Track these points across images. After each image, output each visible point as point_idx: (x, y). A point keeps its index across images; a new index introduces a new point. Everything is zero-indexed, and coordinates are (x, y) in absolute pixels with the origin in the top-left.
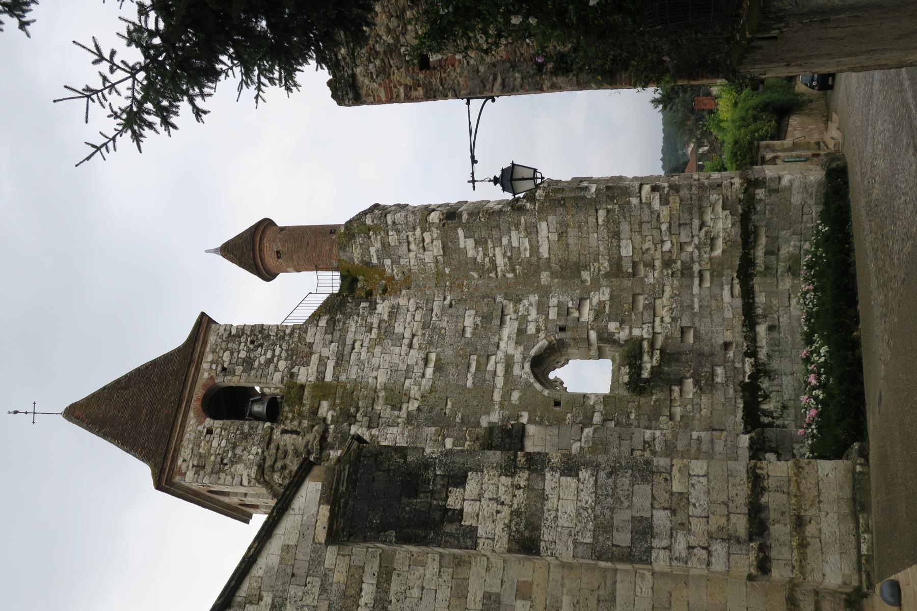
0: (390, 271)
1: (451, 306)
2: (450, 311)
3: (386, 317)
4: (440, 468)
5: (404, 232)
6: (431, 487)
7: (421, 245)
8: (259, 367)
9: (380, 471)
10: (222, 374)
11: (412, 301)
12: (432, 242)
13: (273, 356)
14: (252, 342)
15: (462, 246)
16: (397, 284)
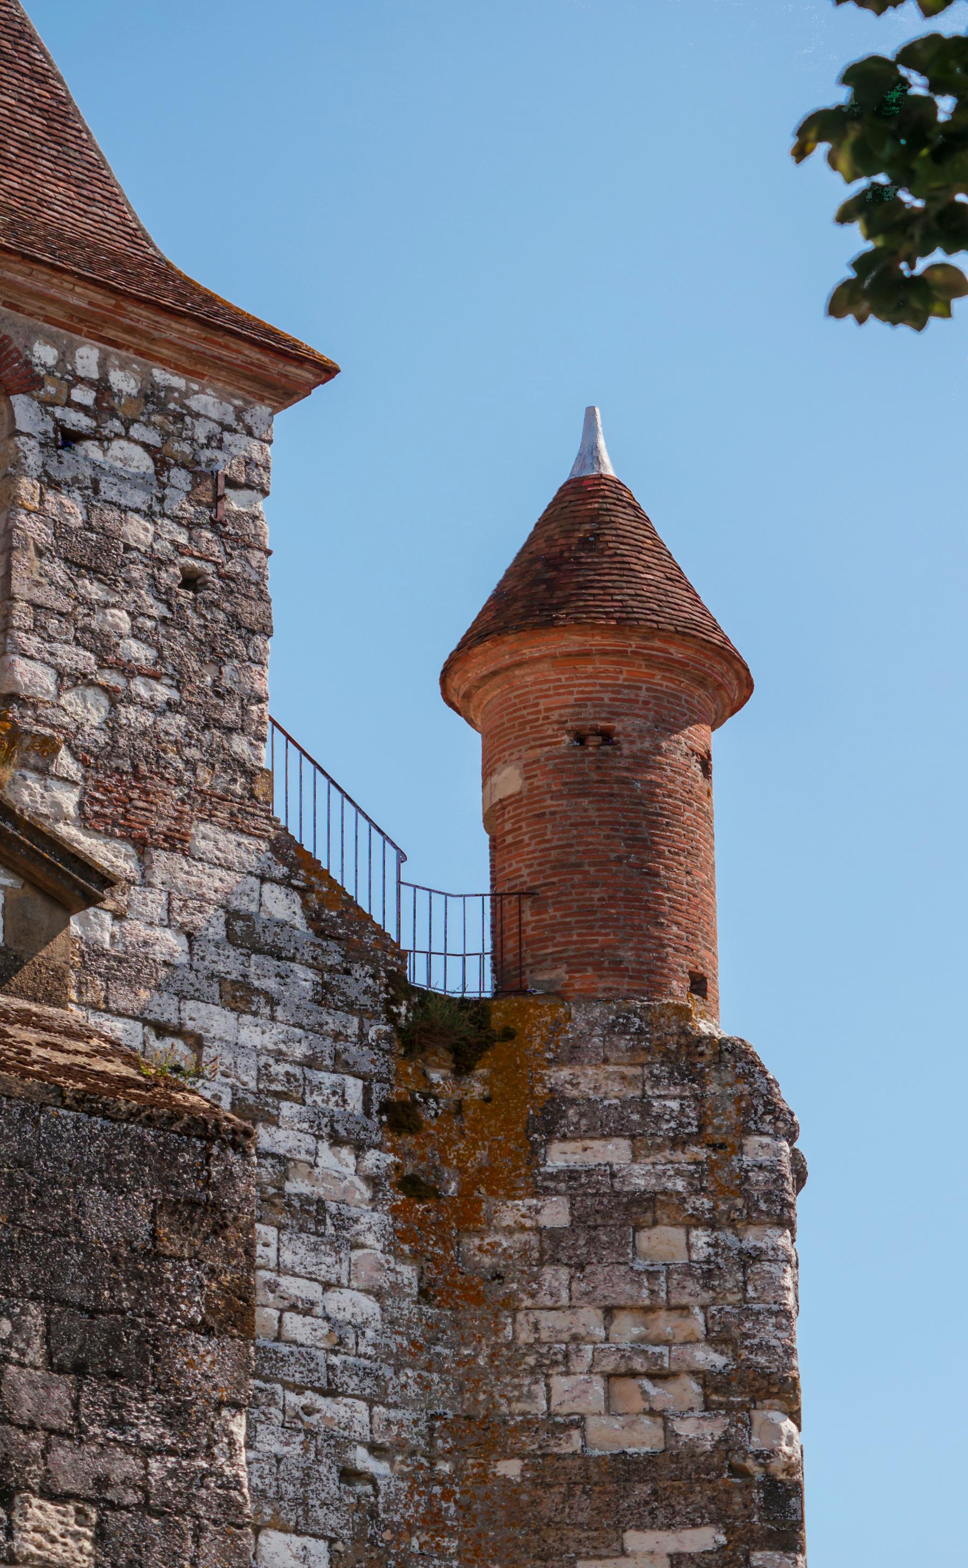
0: (508, 1219)
1: (349, 1475)
2: (327, 1471)
3: (297, 1186)
4: (172, 1473)
5: (707, 1296)
6: (94, 1429)
7: (638, 1364)
8: (82, 601)
9: (153, 1217)
10: (50, 426)
11: (369, 1306)
12: (651, 1412)
13: (128, 670)
14: (191, 581)
15: (634, 1540)
16: (443, 1240)
